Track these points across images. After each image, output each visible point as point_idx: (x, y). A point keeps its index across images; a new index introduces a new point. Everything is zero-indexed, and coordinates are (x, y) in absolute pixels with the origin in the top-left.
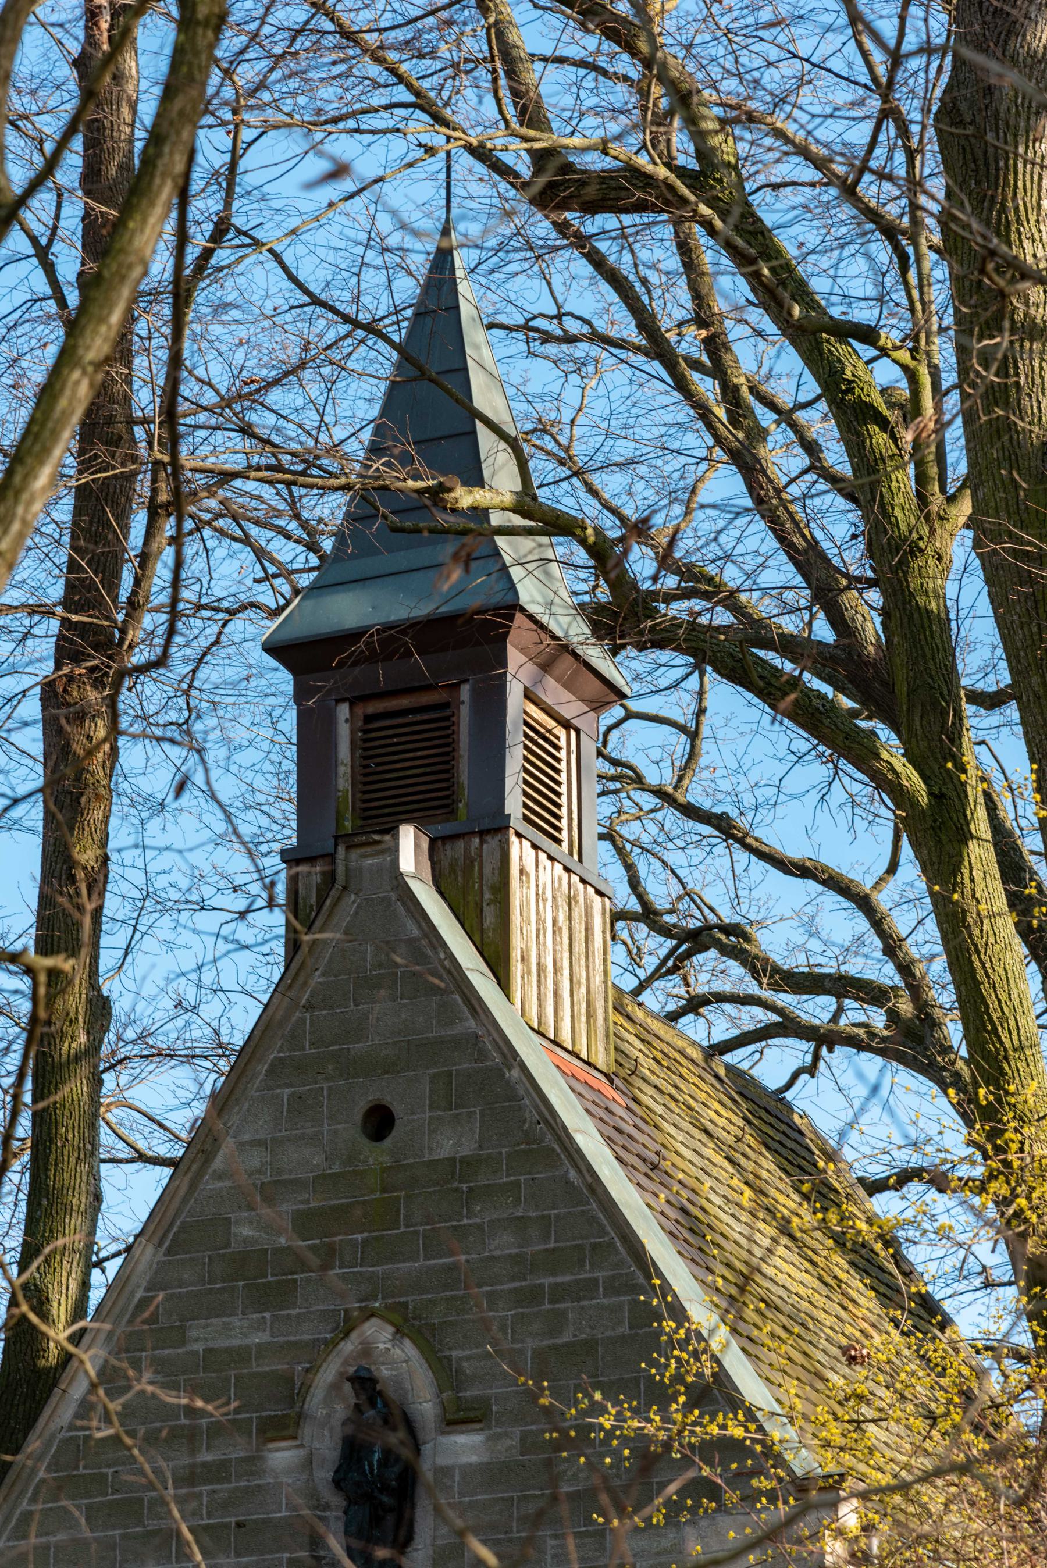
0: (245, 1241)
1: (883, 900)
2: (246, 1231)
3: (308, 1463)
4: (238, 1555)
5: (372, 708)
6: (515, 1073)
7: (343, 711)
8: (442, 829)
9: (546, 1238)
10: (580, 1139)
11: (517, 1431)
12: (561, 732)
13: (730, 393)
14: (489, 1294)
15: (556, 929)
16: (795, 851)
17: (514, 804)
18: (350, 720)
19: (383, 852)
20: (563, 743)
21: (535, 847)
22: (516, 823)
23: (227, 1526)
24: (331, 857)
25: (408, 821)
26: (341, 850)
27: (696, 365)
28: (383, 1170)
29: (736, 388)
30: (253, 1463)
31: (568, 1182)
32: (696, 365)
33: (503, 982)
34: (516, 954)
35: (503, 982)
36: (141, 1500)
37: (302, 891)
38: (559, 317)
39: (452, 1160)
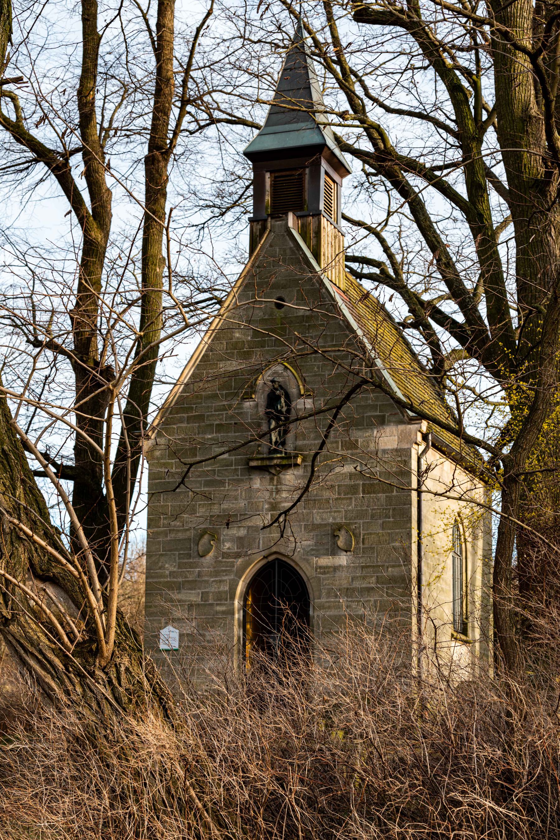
0: (238, 338)
1: (384, 234)
2: (237, 335)
3: (257, 406)
4: (235, 432)
5: (276, 175)
6: (324, 290)
7: (268, 175)
8: (299, 213)
9: (332, 341)
10: (344, 311)
11: (322, 399)
12: (333, 184)
13: (343, 69)
14: (315, 357)
15: (332, 246)
16: (356, 218)
17: (322, 207)
18: (270, 177)
19: (283, 220)
20: (333, 187)
21: (327, 220)
22: (323, 213)
23: (231, 424)
24: (265, 221)
25: (291, 210)
26: (269, 219)
27: (334, 62)
28: (281, 318)
29: (345, 69)
30: (240, 406)
31: (340, 324)
32: (334, 62)
33: (319, 263)
34: (322, 254)
35: (319, 263)
36: (204, 415)
37: (254, 230)
38: (283, 40)
39: (303, 316)
